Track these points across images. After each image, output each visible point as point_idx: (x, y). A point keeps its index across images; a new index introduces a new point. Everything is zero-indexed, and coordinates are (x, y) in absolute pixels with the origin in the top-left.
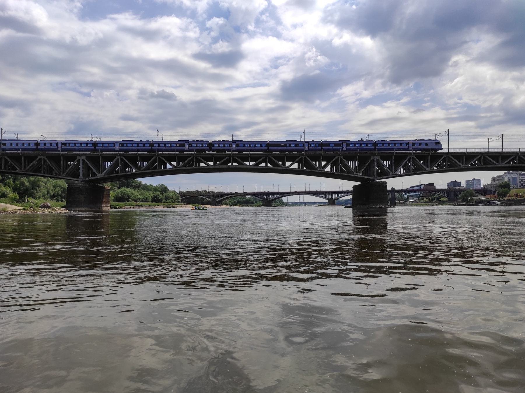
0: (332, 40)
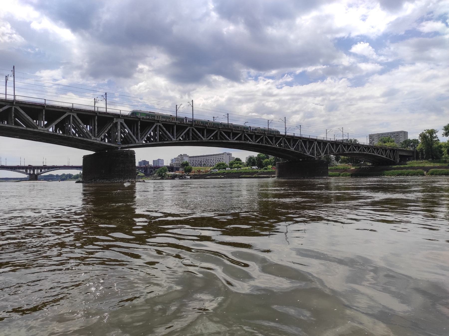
0: (30, 22)
